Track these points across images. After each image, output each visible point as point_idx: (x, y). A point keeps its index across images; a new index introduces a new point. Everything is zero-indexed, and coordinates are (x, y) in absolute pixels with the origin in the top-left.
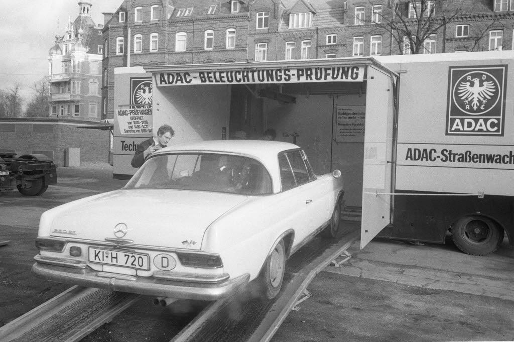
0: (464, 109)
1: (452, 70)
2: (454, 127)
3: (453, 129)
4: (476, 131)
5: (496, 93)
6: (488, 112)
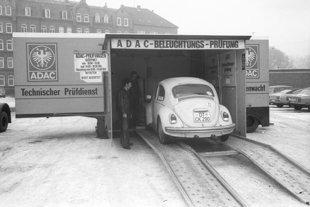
0: (37, 67)
1: (258, 46)
2: (32, 77)
3: (31, 78)
4: (248, 76)
5: (255, 58)
6: (49, 68)
